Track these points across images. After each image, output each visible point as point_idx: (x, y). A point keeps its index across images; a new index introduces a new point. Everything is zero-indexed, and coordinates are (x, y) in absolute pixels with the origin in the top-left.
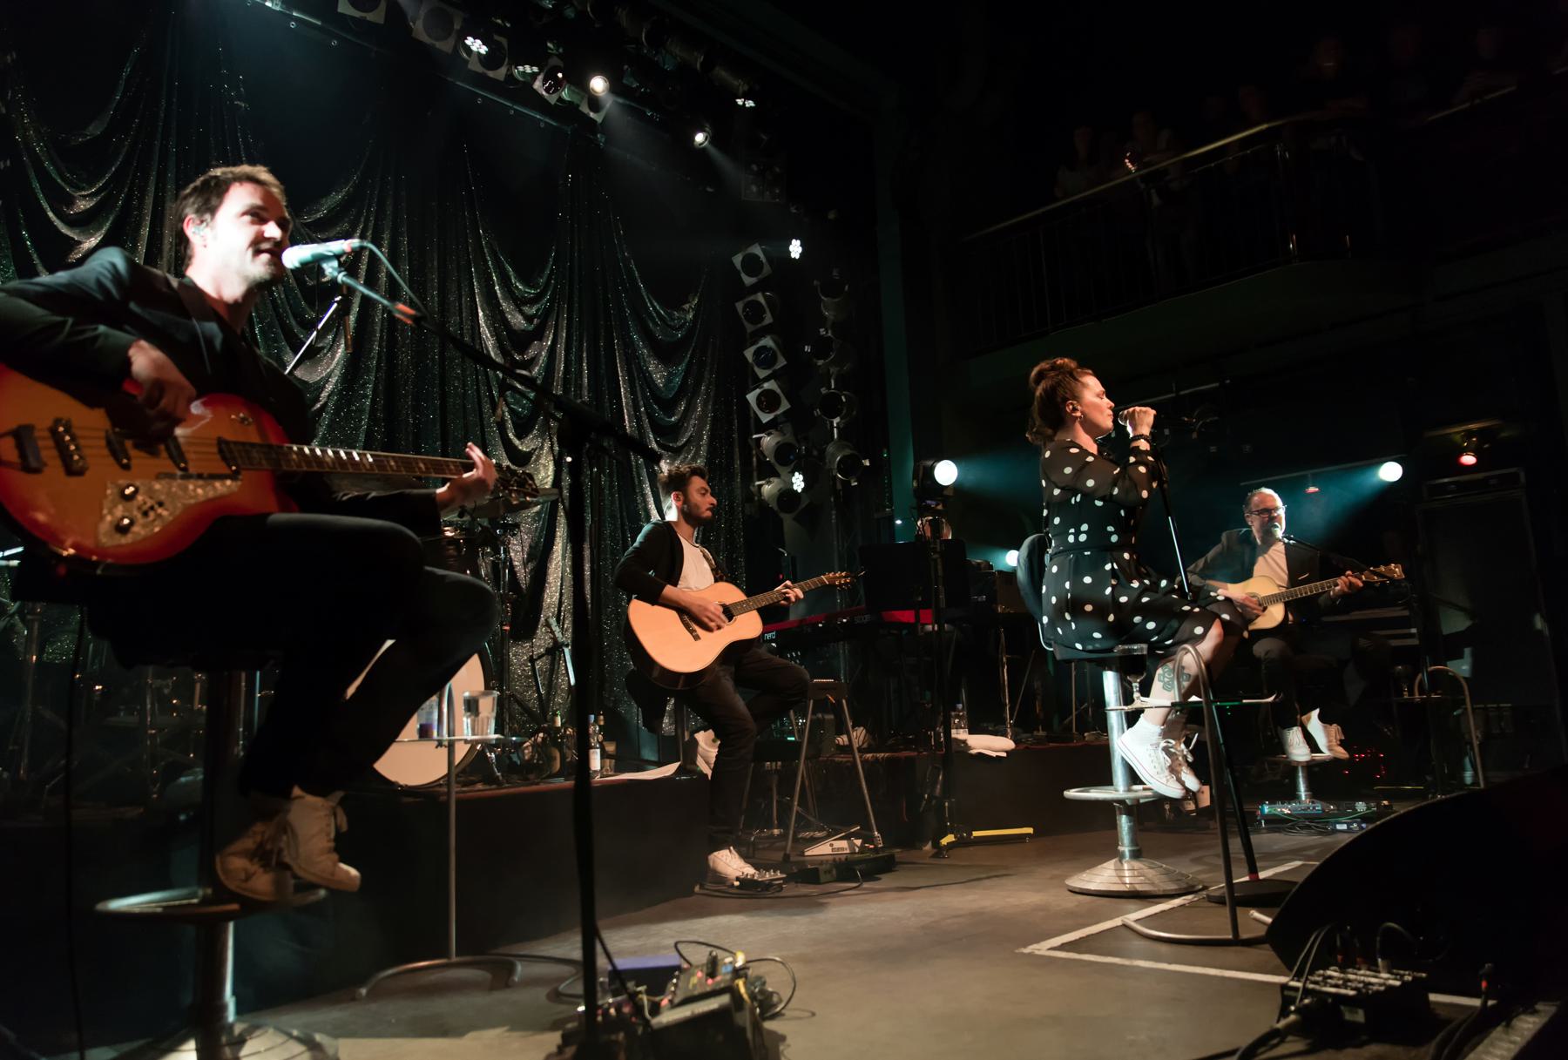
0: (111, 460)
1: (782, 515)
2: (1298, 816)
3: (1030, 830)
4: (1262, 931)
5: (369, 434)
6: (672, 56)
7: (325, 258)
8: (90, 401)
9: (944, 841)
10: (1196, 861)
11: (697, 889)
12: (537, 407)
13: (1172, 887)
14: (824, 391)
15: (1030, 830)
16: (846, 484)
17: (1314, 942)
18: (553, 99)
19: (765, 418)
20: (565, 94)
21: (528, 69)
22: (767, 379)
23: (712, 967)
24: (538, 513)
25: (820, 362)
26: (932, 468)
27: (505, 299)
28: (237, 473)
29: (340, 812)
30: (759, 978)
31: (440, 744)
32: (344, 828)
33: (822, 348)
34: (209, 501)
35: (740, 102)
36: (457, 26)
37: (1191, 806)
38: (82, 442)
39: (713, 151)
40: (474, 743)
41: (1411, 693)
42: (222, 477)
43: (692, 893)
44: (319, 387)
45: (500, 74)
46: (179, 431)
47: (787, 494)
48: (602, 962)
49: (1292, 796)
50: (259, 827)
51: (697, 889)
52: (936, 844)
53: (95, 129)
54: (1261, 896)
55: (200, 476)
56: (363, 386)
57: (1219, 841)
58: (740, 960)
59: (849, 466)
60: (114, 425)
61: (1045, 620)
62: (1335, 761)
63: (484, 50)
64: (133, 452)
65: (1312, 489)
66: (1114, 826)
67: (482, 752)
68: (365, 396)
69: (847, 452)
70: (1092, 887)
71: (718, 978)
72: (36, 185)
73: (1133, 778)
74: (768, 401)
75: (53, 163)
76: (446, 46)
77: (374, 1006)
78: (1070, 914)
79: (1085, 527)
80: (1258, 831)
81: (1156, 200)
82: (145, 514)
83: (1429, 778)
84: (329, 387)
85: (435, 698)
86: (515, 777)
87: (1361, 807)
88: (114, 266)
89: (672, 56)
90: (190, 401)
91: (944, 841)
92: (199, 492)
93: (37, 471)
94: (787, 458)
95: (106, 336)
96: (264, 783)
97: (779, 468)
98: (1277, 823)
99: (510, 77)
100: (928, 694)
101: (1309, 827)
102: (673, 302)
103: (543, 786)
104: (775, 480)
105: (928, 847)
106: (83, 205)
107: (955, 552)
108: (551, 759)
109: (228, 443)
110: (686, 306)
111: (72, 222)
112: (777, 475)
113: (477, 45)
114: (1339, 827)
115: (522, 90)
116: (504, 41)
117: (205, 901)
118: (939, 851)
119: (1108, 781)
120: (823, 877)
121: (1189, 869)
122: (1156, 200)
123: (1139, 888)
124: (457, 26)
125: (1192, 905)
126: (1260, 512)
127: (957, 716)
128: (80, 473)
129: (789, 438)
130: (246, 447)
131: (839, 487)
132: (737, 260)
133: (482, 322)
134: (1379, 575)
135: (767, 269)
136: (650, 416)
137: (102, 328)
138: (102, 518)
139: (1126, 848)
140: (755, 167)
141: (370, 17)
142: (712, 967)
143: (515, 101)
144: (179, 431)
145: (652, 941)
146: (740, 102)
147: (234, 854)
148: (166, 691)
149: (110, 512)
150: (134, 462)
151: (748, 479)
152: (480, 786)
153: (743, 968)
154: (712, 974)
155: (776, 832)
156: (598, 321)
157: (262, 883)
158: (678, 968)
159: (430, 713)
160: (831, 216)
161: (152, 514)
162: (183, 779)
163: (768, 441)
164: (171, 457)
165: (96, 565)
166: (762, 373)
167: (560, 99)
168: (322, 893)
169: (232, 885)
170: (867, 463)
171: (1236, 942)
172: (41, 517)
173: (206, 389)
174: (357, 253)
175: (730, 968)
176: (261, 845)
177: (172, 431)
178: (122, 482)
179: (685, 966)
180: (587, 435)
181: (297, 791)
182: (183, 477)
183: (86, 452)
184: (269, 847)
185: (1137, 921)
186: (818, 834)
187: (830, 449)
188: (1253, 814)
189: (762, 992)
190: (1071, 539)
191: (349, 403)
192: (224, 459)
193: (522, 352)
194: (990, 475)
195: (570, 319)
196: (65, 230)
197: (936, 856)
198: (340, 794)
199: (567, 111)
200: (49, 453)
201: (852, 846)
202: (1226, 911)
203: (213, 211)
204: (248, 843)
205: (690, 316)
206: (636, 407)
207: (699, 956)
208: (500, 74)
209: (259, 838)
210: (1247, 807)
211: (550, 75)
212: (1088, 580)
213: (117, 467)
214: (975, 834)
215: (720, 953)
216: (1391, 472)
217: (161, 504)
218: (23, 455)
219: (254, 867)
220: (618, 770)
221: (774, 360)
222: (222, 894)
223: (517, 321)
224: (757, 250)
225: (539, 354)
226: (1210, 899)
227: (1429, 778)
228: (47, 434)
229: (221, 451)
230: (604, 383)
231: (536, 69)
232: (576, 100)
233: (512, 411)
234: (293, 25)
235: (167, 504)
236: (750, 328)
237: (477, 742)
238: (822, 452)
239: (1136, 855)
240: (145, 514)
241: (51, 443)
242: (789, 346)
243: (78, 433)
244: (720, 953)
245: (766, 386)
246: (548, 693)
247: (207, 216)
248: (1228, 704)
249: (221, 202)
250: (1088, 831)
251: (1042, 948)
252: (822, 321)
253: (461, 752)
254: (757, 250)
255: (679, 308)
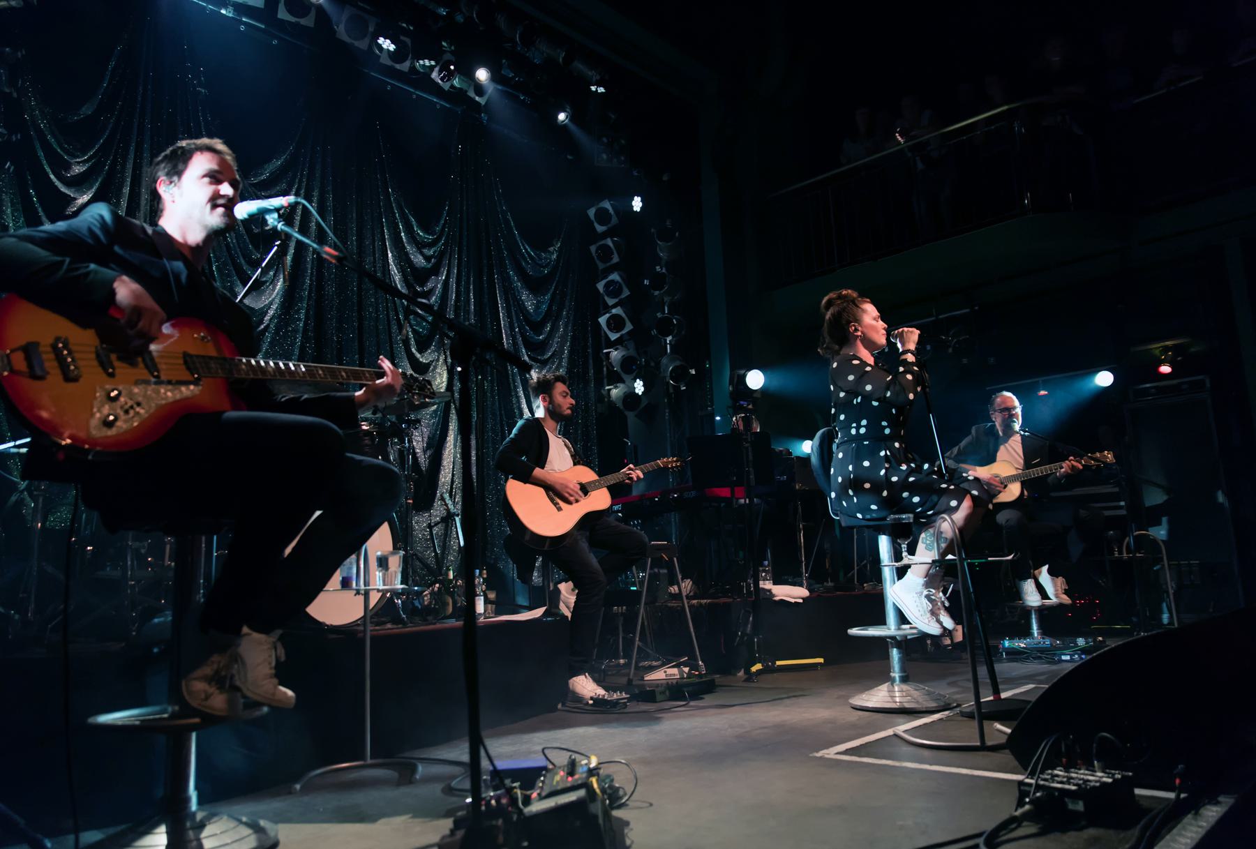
0: (100, 370)
1: (627, 413)
2: (1032, 649)
3: (821, 660)
4: (1003, 740)
5: (302, 348)
6: (540, 53)
7: (268, 211)
8: (83, 324)
9: (754, 669)
10: (951, 684)
11: (560, 706)
12: (434, 328)
13: (933, 705)
14: (659, 315)
15: (821, 660)
16: (677, 388)
17: (1043, 749)
18: (446, 86)
19: (613, 337)
20: (456, 82)
21: (427, 63)
22: (615, 306)
23: (572, 768)
24: (435, 411)
25: (657, 293)
26: (744, 376)
27: (409, 243)
28: (198, 379)
29: (279, 646)
30: (608, 776)
31: (358, 592)
32: (283, 658)
33: (658, 281)
34: (176, 402)
35: (593, 88)
36: (371, 29)
37: (947, 641)
38: (76, 355)
39: (572, 127)
40: (384, 592)
41: (1120, 552)
42: (186, 383)
43: (556, 710)
44: (263, 312)
45: (405, 66)
46: (153, 347)
47: (630, 395)
48: (485, 764)
49: (1027, 633)
50: (215, 658)
51: (560, 706)
52: (748, 671)
53: (87, 110)
54: (1002, 712)
55: (169, 382)
56: (298, 312)
57: (970, 669)
58: (594, 763)
59: (679, 374)
60: (102, 342)
61: (833, 495)
62: (1061, 606)
63: (392, 48)
64: (117, 364)
65: (1042, 392)
66: (887, 657)
67: (391, 599)
68: (299, 320)
69: (678, 363)
70: (870, 705)
71: (576, 777)
72: (41, 154)
73: (902, 619)
74: (616, 323)
75: (54, 136)
76: (362, 44)
77: (306, 799)
78: (853, 726)
79: (864, 422)
80: (1000, 660)
81: (920, 166)
82: (127, 412)
83: (1134, 619)
84: (271, 312)
85: (354, 557)
86: (417, 619)
87: (1081, 642)
88: (102, 217)
89: (540, 53)
90: (162, 323)
91: (754, 669)
92: (169, 394)
93: (41, 378)
94: (630, 368)
95: (96, 272)
96: (219, 623)
97: (624, 376)
98: (1015, 655)
99: (413, 68)
100: (741, 554)
101: (1040, 658)
102: (541, 245)
103: (438, 626)
104: (621, 386)
105: (741, 673)
106: (77, 170)
107: (762, 442)
108: (445, 604)
109: (191, 356)
110: (551, 249)
111: (69, 183)
112: (623, 382)
113: (387, 44)
114: (1064, 658)
115: (422, 80)
116: (408, 40)
117: (173, 716)
118: (750, 677)
119: (882, 621)
120: (659, 697)
121: (946, 690)
122: (920, 166)
123: (907, 705)
124: (371, 29)
125: (948, 719)
126: (1002, 411)
127: (764, 571)
128: (75, 380)
129: (632, 352)
130: (206, 359)
131: (671, 390)
132: (591, 212)
133: (391, 261)
134: (1096, 460)
135: (615, 220)
136: (523, 335)
137: (92, 266)
138: (92, 415)
139: (896, 674)
140: (605, 140)
141: (303, 21)
142: (572, 768)
143: (416, 88)
144: (153, 347)
145: (524, 747)
146: (593, 88)
147: (195, 679)
148: (143, 551)
149: (99, 411)
150: (117, 371)
151: (600, 384)
152: (389, 626)
153: (596, 768)
154: (571, 773)
155: (622, 661)
156: (481, 258)
157: (218, 702)
158: (545, 768)
159: (350, 568)
160: (665, 178)
161: (132, 412)
162: (156, 620)
163: (615, 355)
164: (147, 367)
165: (87, 452)
166: (611, 302)
167: (452, 86)
168: (265, 709)
169: (194, 703)
170: (693, 372)
171: (983, 748)
172: (44, 414)
173: (176, 315)
174: (293, 207)
175: (585, 769)
176: (217, 672)
177: (148, 347)
178: (108, 387)
179: (551, 767)
180: (473, 349)
181: (245, 630)
182: (156, 383)
183: (80, 363)
184: (223, 673)
185: (905, 731)
186: (655, 663)
187: (664, 360)
188: (997, 648)
189: (611, 787)
190: (853, 432)
191: (287, 325)
192: (188, 368)
193: (422, 284)
194: (790, 381)
195: (460, 259)
196: (63, 189)
197: (746, 680)
198: (279, 632)
199: (457, 96)
200: (51, 364)
201: (681, 672)
202: (975, 723)
203: (179, 174)
204: (207, 670)
205: (555, 256)
206: (512, 328)
207: (561, 759)
208: (405, 66)
209: (215, 666)
210: (992, 642)
211: (444, 68)
212: (866, 464)
213: (104, 376)
214: (778, 663)
215: (577, 757)
216: (1104, 379)
217: (139, 404)
218: (31, 366)
219: (212, 690)
220: (498, 613)
221: (620, 291)
222: (187, 710)
223: (419, 260)
224: (607, 205)
225: (436, 287)
226: (963, 714)
227: (1134, 619)
228: (49, 349)
229: (186, 362)
230: (487, 309)
231: (433, 63)
232: (465, 86)
233: (414, 331)
234: (242, 28)
235: (144, 404)
236: (601, 266)
237: (387, 591)
238: (658, 364)
239: (904, 680)
240: (127, 412)
241: (52, 356)
242: (632, 279)
243: (73, 348)
244: (577, 757)
245: (614, 311)
246: (443, 553)
247: (175, 178)
248: (976, 561)
249: (186, 167)
250: (867, 661)
251: (831, 753)
252: (658, 260)
253: (374, 598)
254: (607, 205)
255: (546, 251)
